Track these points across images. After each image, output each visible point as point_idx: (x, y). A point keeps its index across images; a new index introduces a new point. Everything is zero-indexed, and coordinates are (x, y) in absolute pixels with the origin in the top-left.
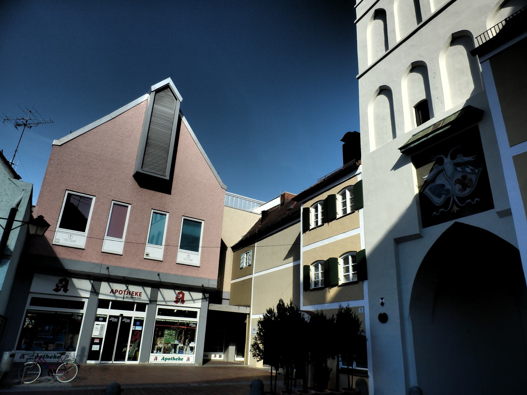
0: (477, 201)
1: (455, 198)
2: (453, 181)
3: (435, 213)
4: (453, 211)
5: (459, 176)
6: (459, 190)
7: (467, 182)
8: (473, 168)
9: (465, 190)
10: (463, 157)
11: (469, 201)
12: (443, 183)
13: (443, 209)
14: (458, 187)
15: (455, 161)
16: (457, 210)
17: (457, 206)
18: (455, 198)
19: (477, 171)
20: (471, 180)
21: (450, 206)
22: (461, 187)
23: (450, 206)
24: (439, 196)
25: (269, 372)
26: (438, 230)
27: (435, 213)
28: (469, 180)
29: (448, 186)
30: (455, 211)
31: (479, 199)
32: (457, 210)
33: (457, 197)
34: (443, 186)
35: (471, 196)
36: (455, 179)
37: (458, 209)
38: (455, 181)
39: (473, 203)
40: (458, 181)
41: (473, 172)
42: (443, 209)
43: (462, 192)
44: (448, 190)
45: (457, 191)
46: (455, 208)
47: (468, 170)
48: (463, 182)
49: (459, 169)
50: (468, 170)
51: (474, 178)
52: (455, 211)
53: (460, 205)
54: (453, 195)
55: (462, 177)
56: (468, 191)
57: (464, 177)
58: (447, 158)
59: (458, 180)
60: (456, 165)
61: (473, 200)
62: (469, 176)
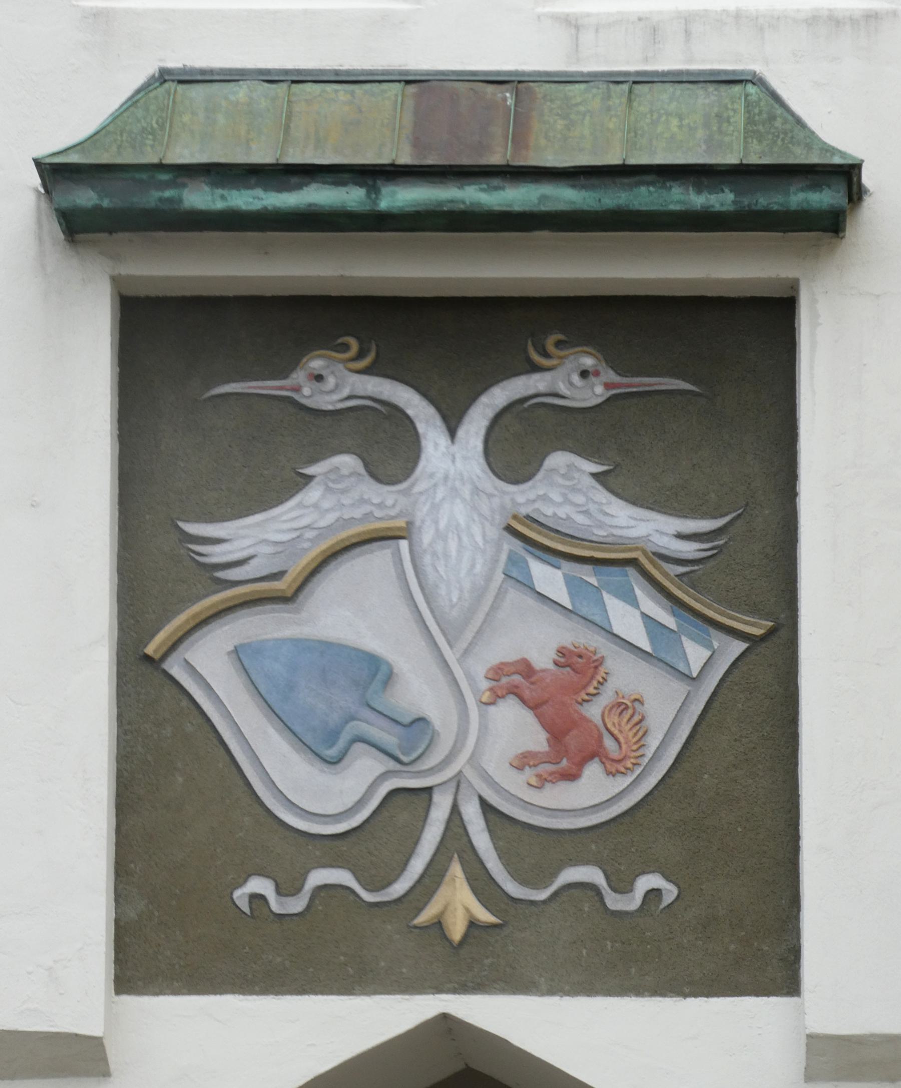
0: (654, 894)
1: (472, 813)
2: (480, 668)
3: (259, 885)
4: (438, 925)
5: (538, 640)
6: (523, 761)
7: (594, 711)
8: (669, 621)
9: (571, 776)
10: (601, 495)
11: (592, 874)
12: (372, 644)
13: (342, 877)
14: (515, 728)
15: (523, 497)
16: (473, 924)
17: (482, 884)
18: (472, 813)
19: (696, 655)
20: (628, 707)
21: (417, 866)
22: (536, 739)
23: (417, 866)
24: (326, 748)
25: (520, 140)
26: (309, 471)
27: (259, 885)
28: (620, 707)
29: (418, 690)
30: (457, 930)
31: (670, 892)
32: (473, 924)
33: (486, 807)
34: (373, 671)
35: (617, 840)
36: (503, 648)
37: (484, 916)
38: (497, 672)
39: (614, 902)
40: (515, 681)
41: (660, 656)
42: (342, 877)
43: (542, 782)
44: (421, 721)
45: (496, 762)
46: (458, 904)
47: (626, 620)
48: (563, 706)
49: (549, 578)
50: (626, 620)
51: (666, 710)
52: (457, 930)
53: (513, 888)
54: (458, 781)
55: (567, 657)
56: (593, 795)
57: (580, 667)
58: (452, 424)
59: (526, 669)
60: (531, 537)
61: (623, 886)
62: (625, 676)
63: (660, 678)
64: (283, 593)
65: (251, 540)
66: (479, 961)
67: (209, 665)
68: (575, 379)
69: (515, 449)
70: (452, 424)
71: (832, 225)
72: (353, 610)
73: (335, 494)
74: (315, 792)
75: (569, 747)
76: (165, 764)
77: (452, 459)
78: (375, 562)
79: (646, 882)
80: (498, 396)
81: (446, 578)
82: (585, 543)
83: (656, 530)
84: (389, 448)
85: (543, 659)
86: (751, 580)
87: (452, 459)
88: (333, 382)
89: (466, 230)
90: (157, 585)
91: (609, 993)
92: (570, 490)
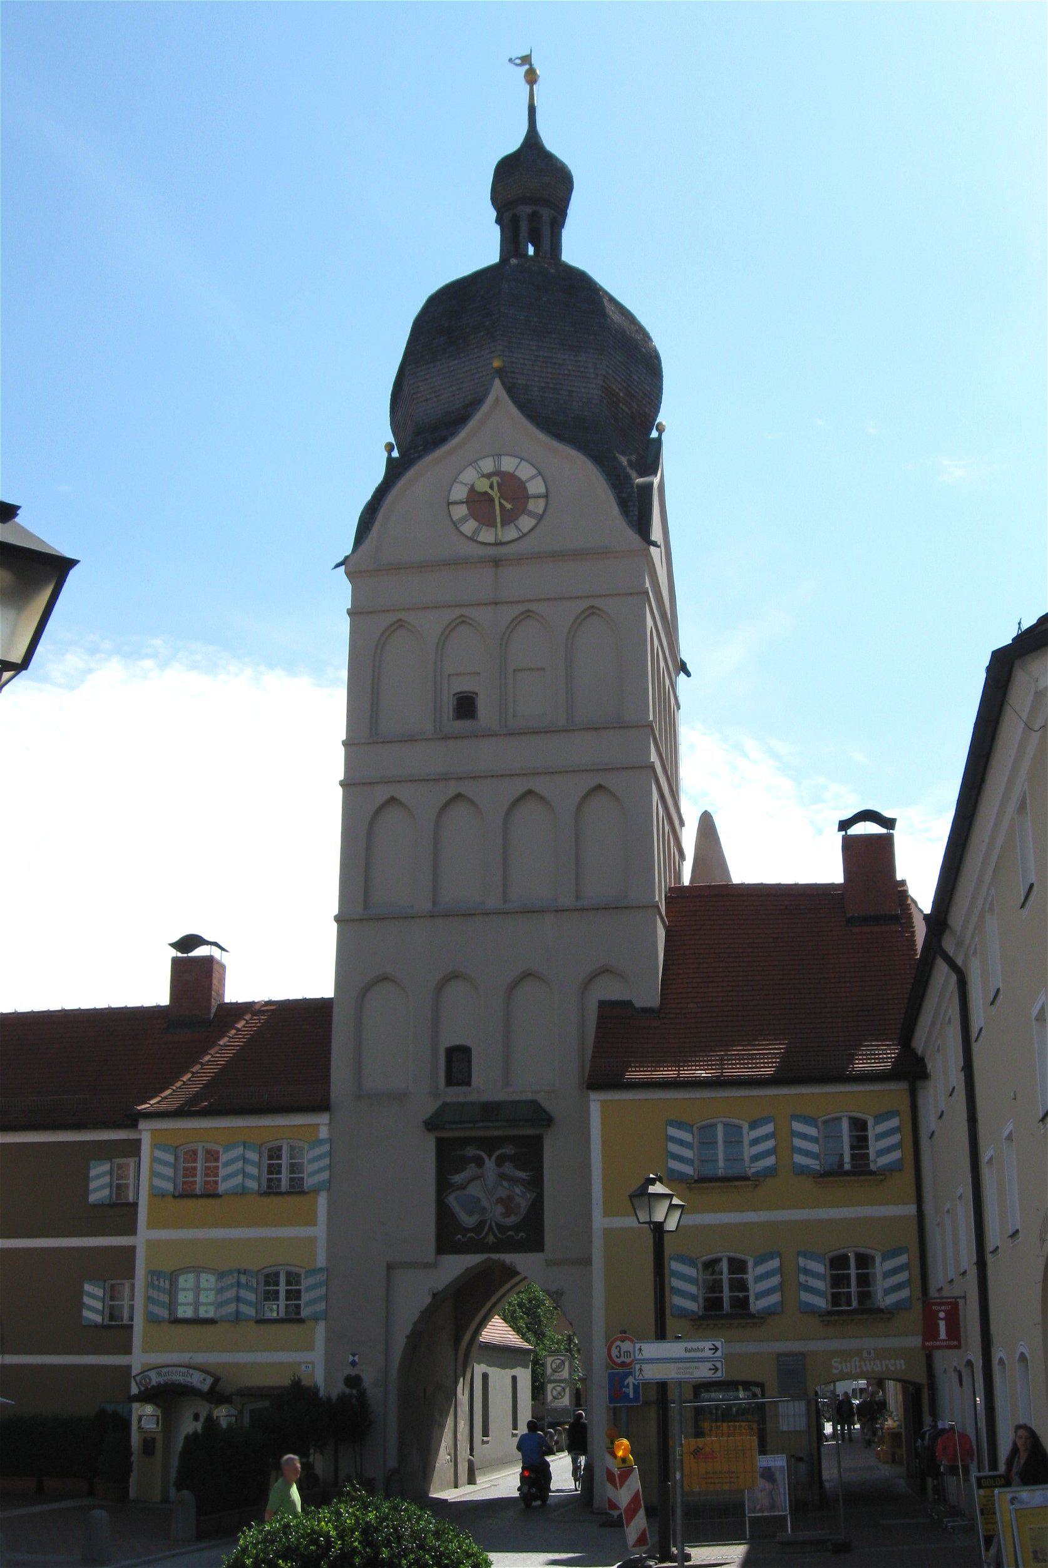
5: (502, 1193)
14: (500, 1209)
15: (501, 1170)
17: (495, 1236)
24: (470, 1213)
29: (485, 1203)
35: (517, 1228)
40: (500, 1201)
46: (491, 1239)
47: (517, 1190)
48: (507, 1203)
49: (505, 1184)
56: (512, 1220)
57: (510, 1198)
58: (490, 1156)
60: (502, 1176)
63: (523, 1201)
64: (463, 1187)
65: (458, 1178)
66: (498, 1248)
67: (451, 1200)
68: (509, 1150)
69: (500, 1162)
70: (490, 1156)
71: (549, 1125)
72: (475, 1190)
73: (471, 1170)
74: (468, 1220)
75: (508, 1212)
76: (444, 1216)
77: (490, 1164)
78: (478, 1182)
79: (521, 1234)
80: (497, 1153)
81: (487, 1189)
82: (1018, 1552)
83: (522, 1175)
84: (480, 1162)
85: (504, 1196)
86: (536, 1183)
87: (490, 1164)
88: (471, 1151)
89: (542, 1225)
90: (443, 1186)
91: (557, 159)
92: (508, 1168)
